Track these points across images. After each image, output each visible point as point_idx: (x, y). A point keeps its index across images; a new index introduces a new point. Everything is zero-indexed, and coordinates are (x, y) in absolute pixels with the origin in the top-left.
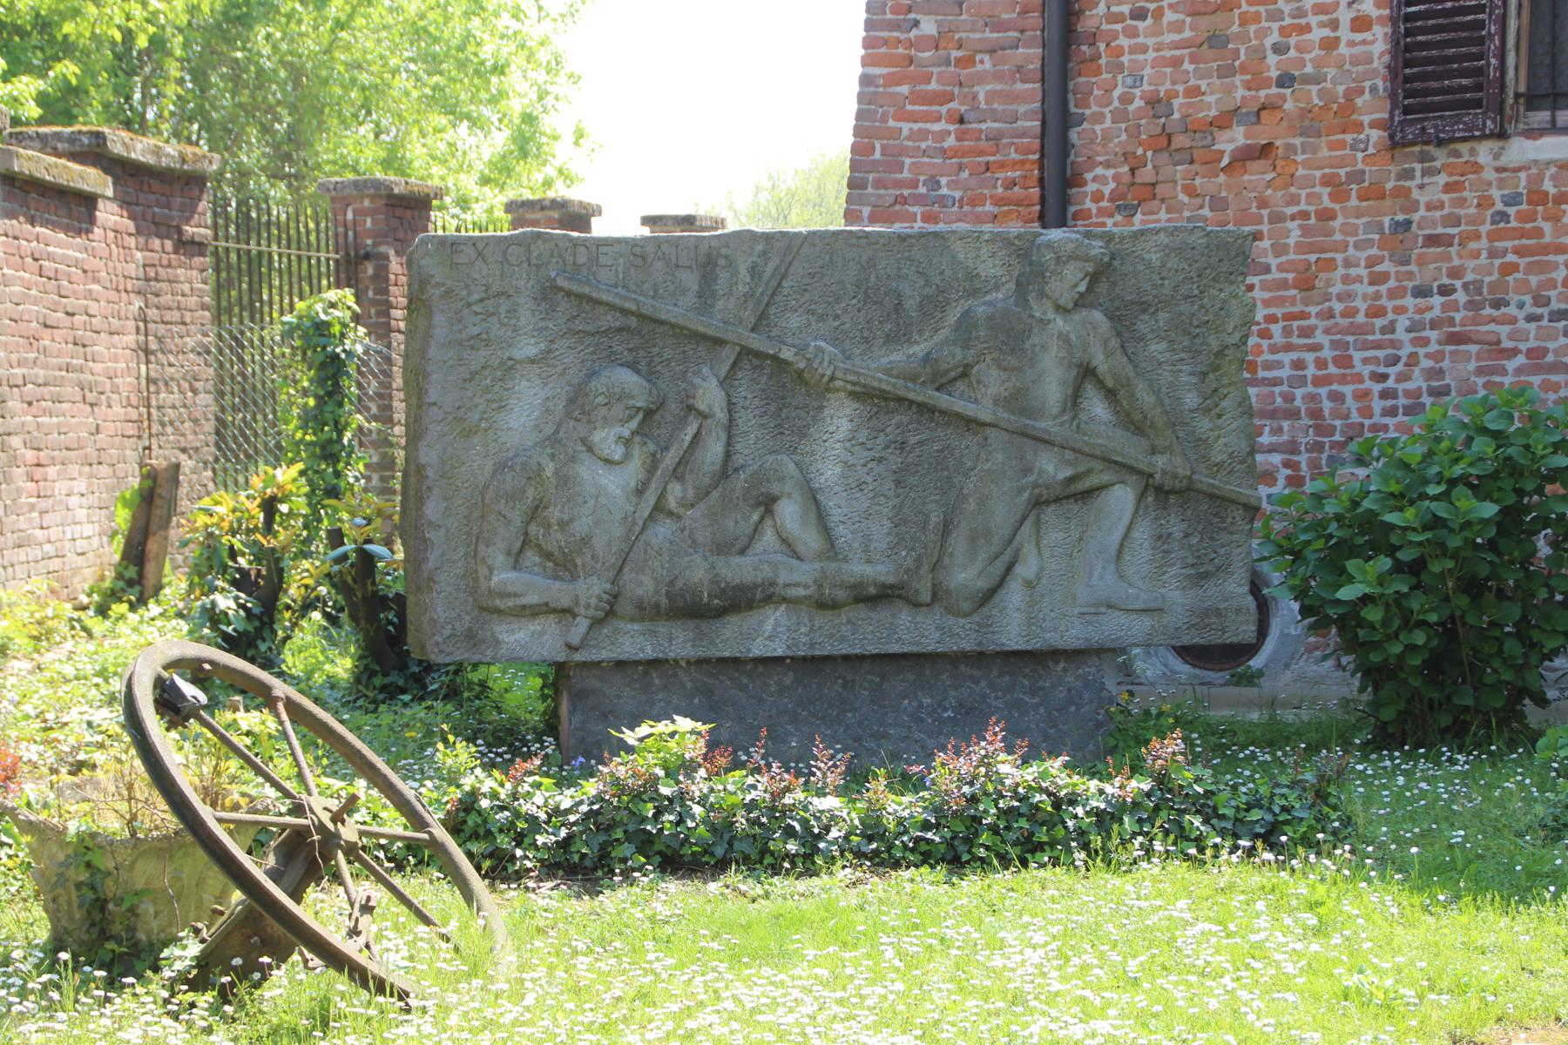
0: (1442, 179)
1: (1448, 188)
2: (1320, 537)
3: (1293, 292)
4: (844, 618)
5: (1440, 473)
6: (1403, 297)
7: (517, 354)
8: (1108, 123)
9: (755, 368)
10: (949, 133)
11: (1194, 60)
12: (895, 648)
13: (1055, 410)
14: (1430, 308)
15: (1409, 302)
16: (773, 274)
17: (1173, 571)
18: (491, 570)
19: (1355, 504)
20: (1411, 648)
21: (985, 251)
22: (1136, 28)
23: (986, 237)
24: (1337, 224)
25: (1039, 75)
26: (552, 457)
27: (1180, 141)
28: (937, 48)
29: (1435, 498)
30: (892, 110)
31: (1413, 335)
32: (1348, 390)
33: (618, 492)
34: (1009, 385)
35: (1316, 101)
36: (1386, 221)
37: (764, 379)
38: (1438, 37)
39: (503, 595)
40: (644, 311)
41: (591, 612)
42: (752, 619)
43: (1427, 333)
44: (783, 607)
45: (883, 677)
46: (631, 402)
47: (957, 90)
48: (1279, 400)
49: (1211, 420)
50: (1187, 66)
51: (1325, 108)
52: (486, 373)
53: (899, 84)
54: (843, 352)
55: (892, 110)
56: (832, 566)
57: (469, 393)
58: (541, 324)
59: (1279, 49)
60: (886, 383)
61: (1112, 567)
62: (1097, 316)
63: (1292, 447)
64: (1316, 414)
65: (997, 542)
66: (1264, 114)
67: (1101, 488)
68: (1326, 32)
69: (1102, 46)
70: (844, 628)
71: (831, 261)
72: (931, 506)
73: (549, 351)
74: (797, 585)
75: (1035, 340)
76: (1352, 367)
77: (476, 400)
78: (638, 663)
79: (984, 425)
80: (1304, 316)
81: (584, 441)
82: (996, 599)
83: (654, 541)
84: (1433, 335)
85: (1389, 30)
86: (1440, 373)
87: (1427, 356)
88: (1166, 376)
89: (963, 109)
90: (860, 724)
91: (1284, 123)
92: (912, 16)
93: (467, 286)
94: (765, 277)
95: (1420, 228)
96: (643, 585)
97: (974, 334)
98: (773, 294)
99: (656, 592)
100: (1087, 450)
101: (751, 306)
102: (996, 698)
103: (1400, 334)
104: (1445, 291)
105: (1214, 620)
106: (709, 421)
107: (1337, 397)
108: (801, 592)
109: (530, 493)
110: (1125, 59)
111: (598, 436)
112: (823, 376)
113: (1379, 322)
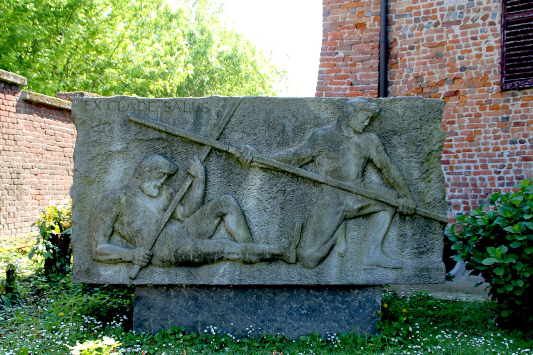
0: (520, 102)
1: (522, 105)
2: (475, 235)
3: (466, 142)
4: (256, 269)
5: (530, 209)
6: (506, 144)
7: (113, 149)
8: (401, 84)
9: (218, 156)
10: (347, 89)
11: (431, 62)
12: (279, 283)
13: (354, 177)
14: (516, 148)
15: (508, 146)
16: (227, 115)
17: (408, 250)
18: (97, 243)
19: (491, 221)
20: (517, 288)
21: (323, 107)
22: (410, 52)
23: (324, 101)
24: (482, 118)
25: (377, 69)
26: (125, 194)
27: (426, 90)
28: (344, 61)
29: (527, 221)
30: (329, 81)
31: (510, 157)
32: (486, 177)
33: (155, 210)
34: (332, 166)
35: (474, 76)
36: (500, 117)
37: (222, 161)
38: (518, 52)
39: (102, 254)
40: (169, 131)
41: (140, 263)
42: (213, 268)
43: (515, 157)
44: (228, 263)
45: (275, 294)
46: (161, 171)
47: (350, 74)
48: (461, 180)
49: (425, 183)
50: (428, 65)
51: (477, 78)
52: (99, 157)
53: (331, 73)
54: (258, 150)
55: (329, 81)
56: (250, 245)
57: (91, 166)
58: (124, 136)
59: (460, 58)
60: (276, 164)
61: (379, 248)
62: (373, 136)
63: (466, 196)
64: (474, 185)
66: (455, 80)
67: (374, 213)
68: (478, 52)
69: (399, 59)
70: (255, 273)
71: (253, 110)
72: (296, 219)
73: (127, 148)
74: (234, 253)
75: (344, 146)
76: (487, 169)
77: (94, 169)
78: (163, 286)
79: (321, 183)
80: (470, 150)
81: (140, 187)
82: (326, 261)
83: (170, 232)
84: (517, 158)
85: (500, 51)
86: (520, 171)
87: (515, 165)
88: (405, 164)
89: (352, 80)
90: (264, 315)
91: (463, 84)
92: (336, 51)
93: (92, 119)
94: (223, 117)
95: (512, 119)
97: (317, 143)
98: (227, 124)
99: (170, 255)
100: (368, 195)
101: (216, 129)
102: (326, 305)
103: (505, 157)
104: (522, 142)
105: (426, 273)
106: (196, 179)
107: (482, 179)
108: (235, 256)
109: (115, 210)
110: (407, 63)
111: (146, 185)
112: (247, 160)
113: (497, 153)
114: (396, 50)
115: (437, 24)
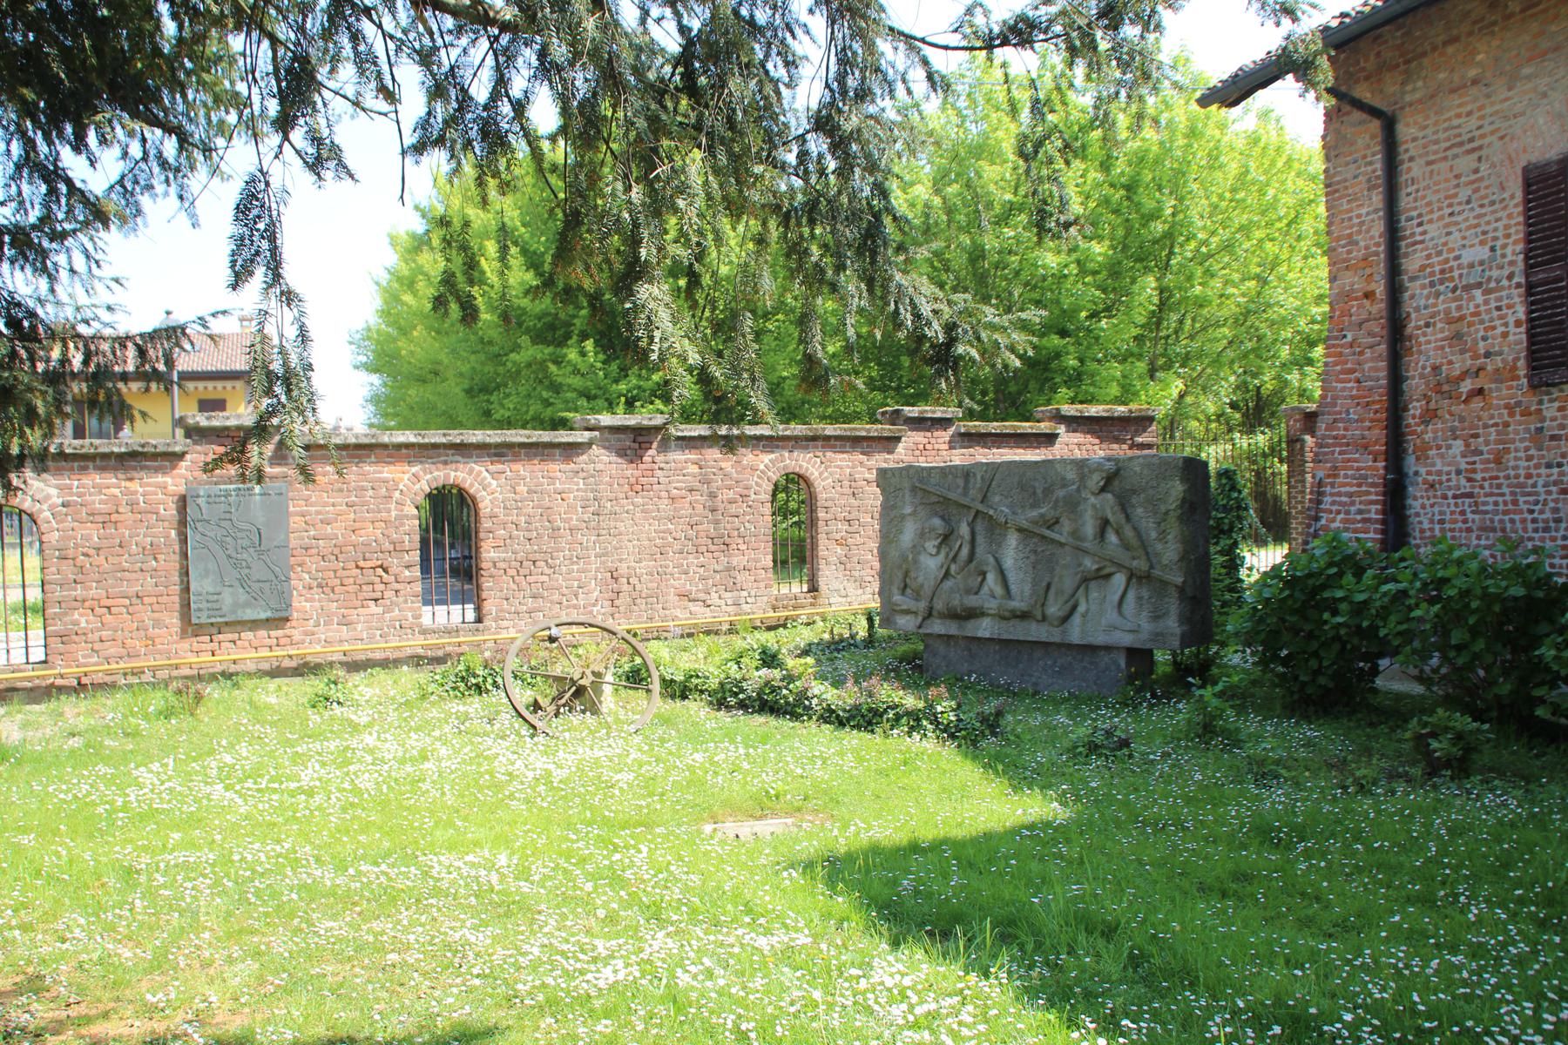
13: (1090, 537)
15: (1543, 471)
32: (1517, 517)
42: (979, 621)
59: (1484, 339)
64: (1503, 530)
65: (1066, 596)
80: (1497, 478)
84: (1554, 489)
96: (939, 605)
103: (1540, 489)
107: (1512, 521)
113: (1530, 482)
114: (1410, 329)
115: (1454, 290)
